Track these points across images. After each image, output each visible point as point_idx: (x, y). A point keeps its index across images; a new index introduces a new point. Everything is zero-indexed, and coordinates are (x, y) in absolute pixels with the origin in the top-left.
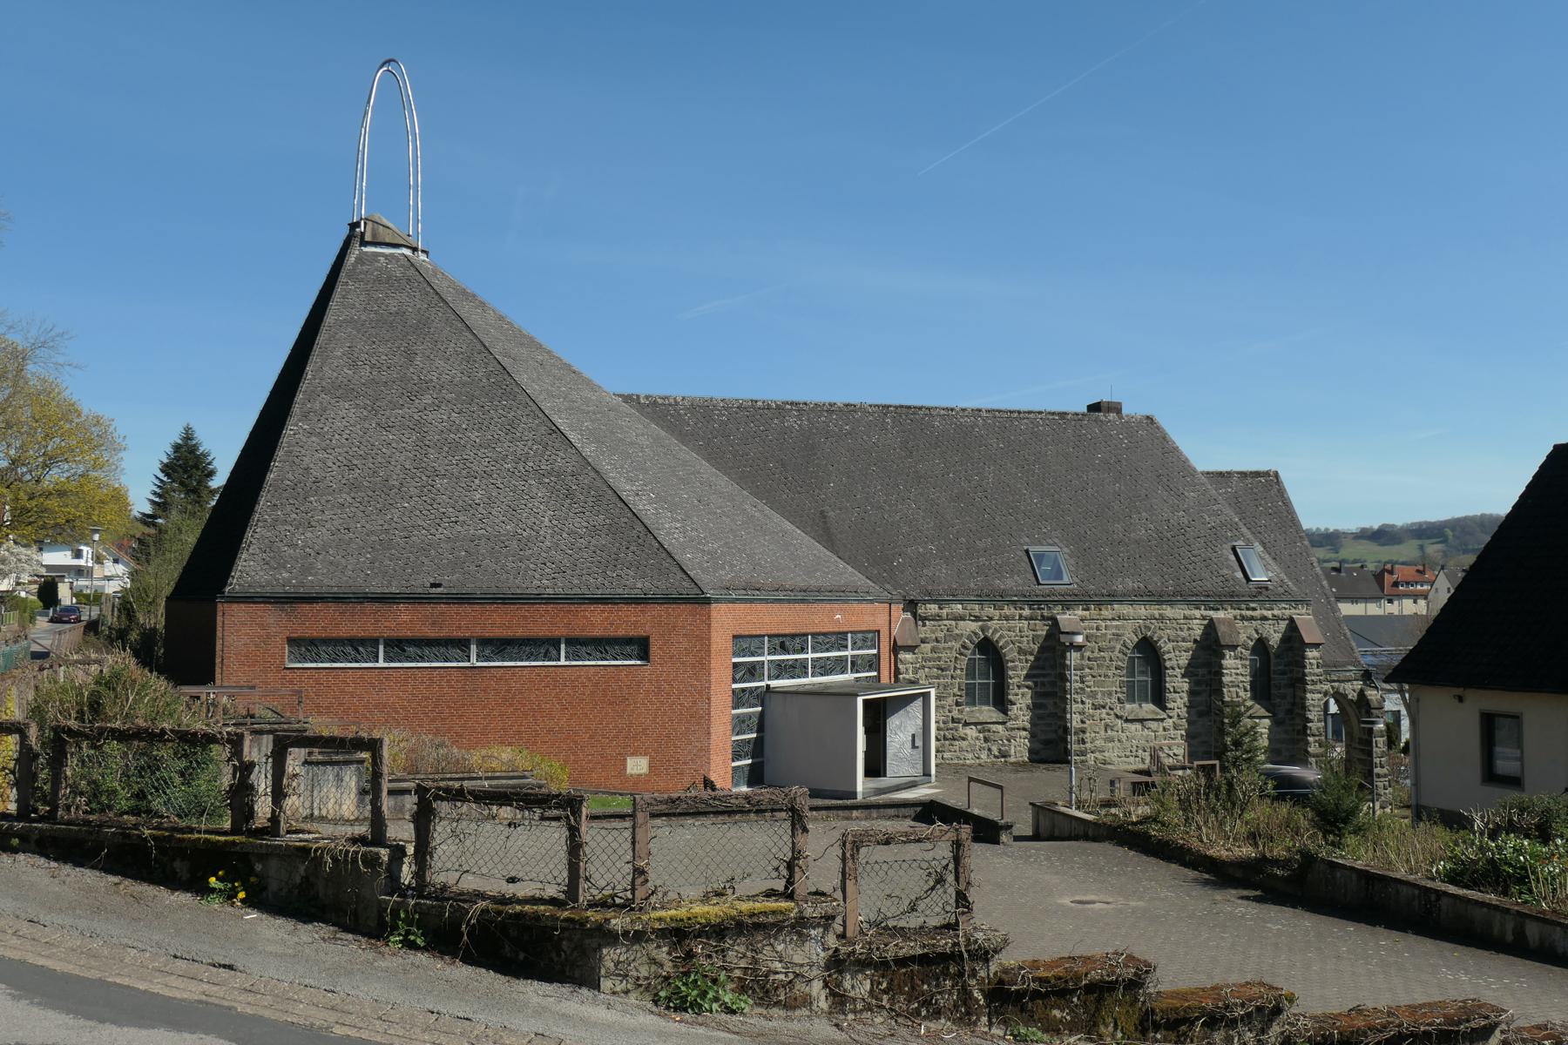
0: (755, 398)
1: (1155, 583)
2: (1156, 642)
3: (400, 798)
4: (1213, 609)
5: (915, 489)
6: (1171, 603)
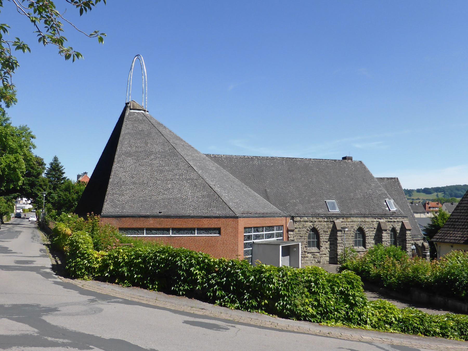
0: (244, 155)
1: (363, 211)
2: (363, 229)
4: (380, 219)
6: (368, 217)
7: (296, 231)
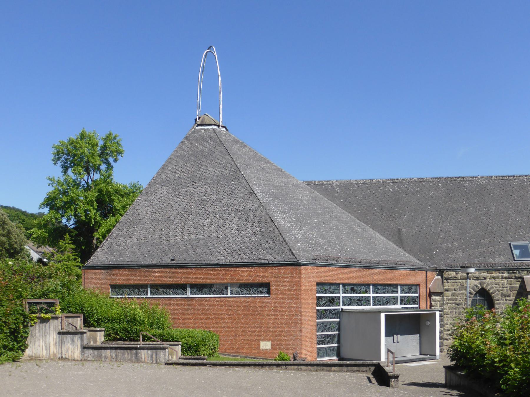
3: (100, 351)
5: (451, 216)
7: (448, 295)
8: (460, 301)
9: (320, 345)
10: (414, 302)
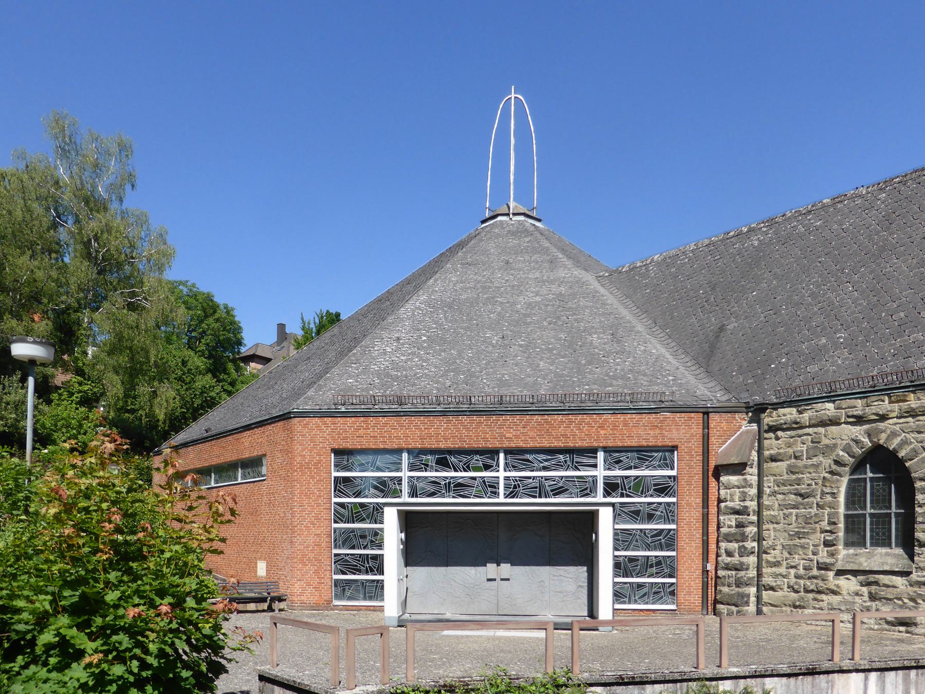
7: (777, 471)
8: (808, 485)
9: (347, 574)
10: (662, 489)
